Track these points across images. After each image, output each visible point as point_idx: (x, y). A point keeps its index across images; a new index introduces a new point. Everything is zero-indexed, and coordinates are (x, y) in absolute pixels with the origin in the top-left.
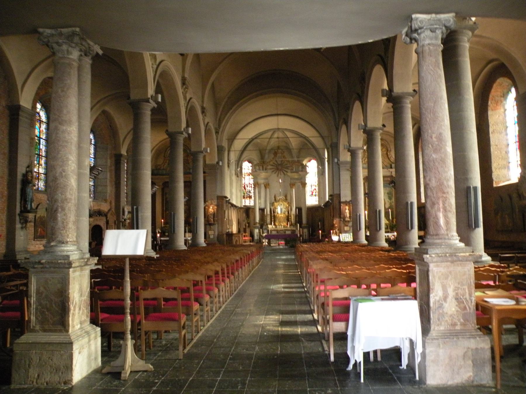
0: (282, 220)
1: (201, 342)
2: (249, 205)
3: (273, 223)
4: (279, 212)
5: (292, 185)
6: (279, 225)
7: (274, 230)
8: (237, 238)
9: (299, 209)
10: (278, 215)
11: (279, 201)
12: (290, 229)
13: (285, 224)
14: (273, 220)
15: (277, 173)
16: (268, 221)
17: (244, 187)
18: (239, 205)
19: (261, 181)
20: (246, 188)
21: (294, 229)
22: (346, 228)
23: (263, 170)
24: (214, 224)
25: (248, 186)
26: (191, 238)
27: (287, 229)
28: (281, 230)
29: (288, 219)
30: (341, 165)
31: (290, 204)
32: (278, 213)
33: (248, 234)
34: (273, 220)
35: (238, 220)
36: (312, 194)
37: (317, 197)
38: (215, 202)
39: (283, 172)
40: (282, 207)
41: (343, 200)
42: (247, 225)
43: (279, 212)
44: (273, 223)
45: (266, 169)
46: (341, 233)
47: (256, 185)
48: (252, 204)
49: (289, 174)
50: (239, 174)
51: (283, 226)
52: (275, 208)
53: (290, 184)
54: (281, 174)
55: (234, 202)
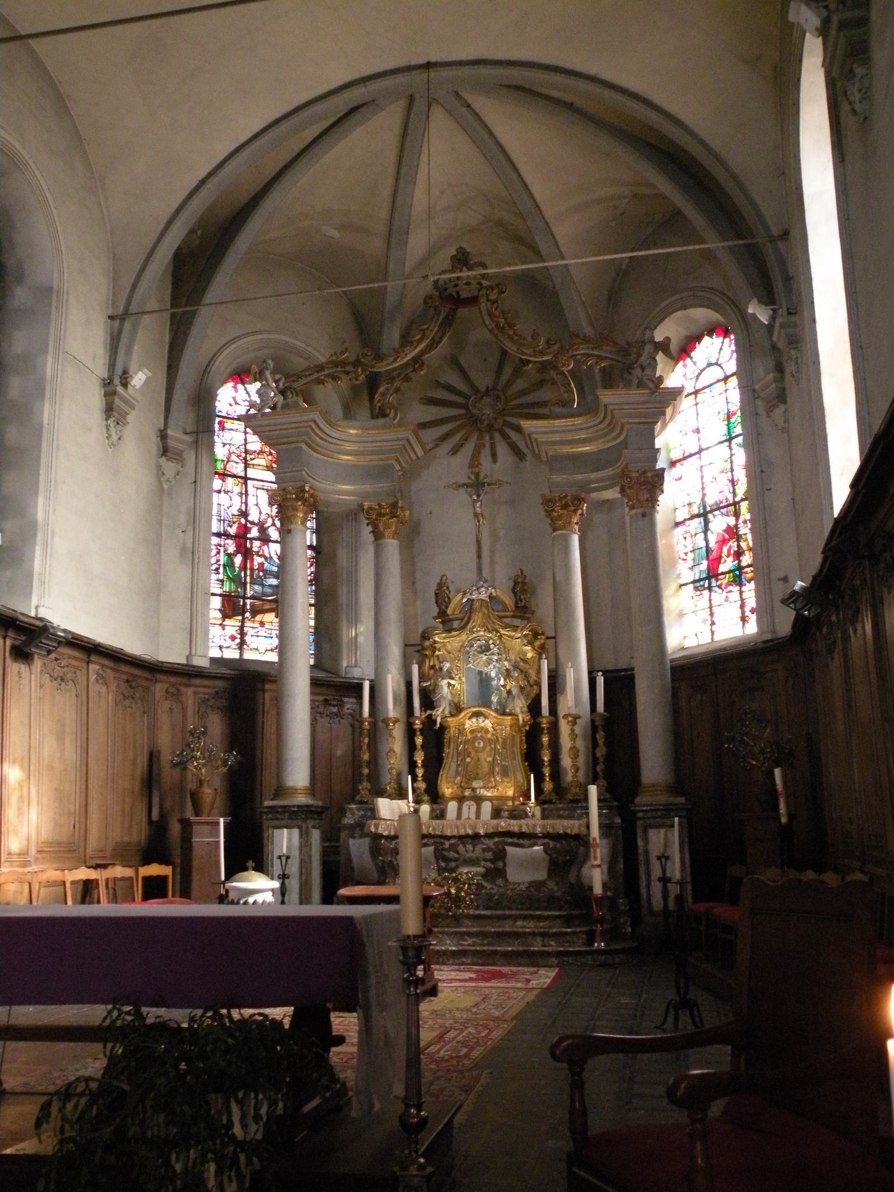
0: (486, 758)
6: (461, 800)
11: (464, 624)
15: (468, 449)
17: (241, 537)
26: (432, 833)
35: (153, 757)
36: (713, 573)
39: (505, 437)
51: (487, 807)
53: (548, 503)
54: (494, 456)
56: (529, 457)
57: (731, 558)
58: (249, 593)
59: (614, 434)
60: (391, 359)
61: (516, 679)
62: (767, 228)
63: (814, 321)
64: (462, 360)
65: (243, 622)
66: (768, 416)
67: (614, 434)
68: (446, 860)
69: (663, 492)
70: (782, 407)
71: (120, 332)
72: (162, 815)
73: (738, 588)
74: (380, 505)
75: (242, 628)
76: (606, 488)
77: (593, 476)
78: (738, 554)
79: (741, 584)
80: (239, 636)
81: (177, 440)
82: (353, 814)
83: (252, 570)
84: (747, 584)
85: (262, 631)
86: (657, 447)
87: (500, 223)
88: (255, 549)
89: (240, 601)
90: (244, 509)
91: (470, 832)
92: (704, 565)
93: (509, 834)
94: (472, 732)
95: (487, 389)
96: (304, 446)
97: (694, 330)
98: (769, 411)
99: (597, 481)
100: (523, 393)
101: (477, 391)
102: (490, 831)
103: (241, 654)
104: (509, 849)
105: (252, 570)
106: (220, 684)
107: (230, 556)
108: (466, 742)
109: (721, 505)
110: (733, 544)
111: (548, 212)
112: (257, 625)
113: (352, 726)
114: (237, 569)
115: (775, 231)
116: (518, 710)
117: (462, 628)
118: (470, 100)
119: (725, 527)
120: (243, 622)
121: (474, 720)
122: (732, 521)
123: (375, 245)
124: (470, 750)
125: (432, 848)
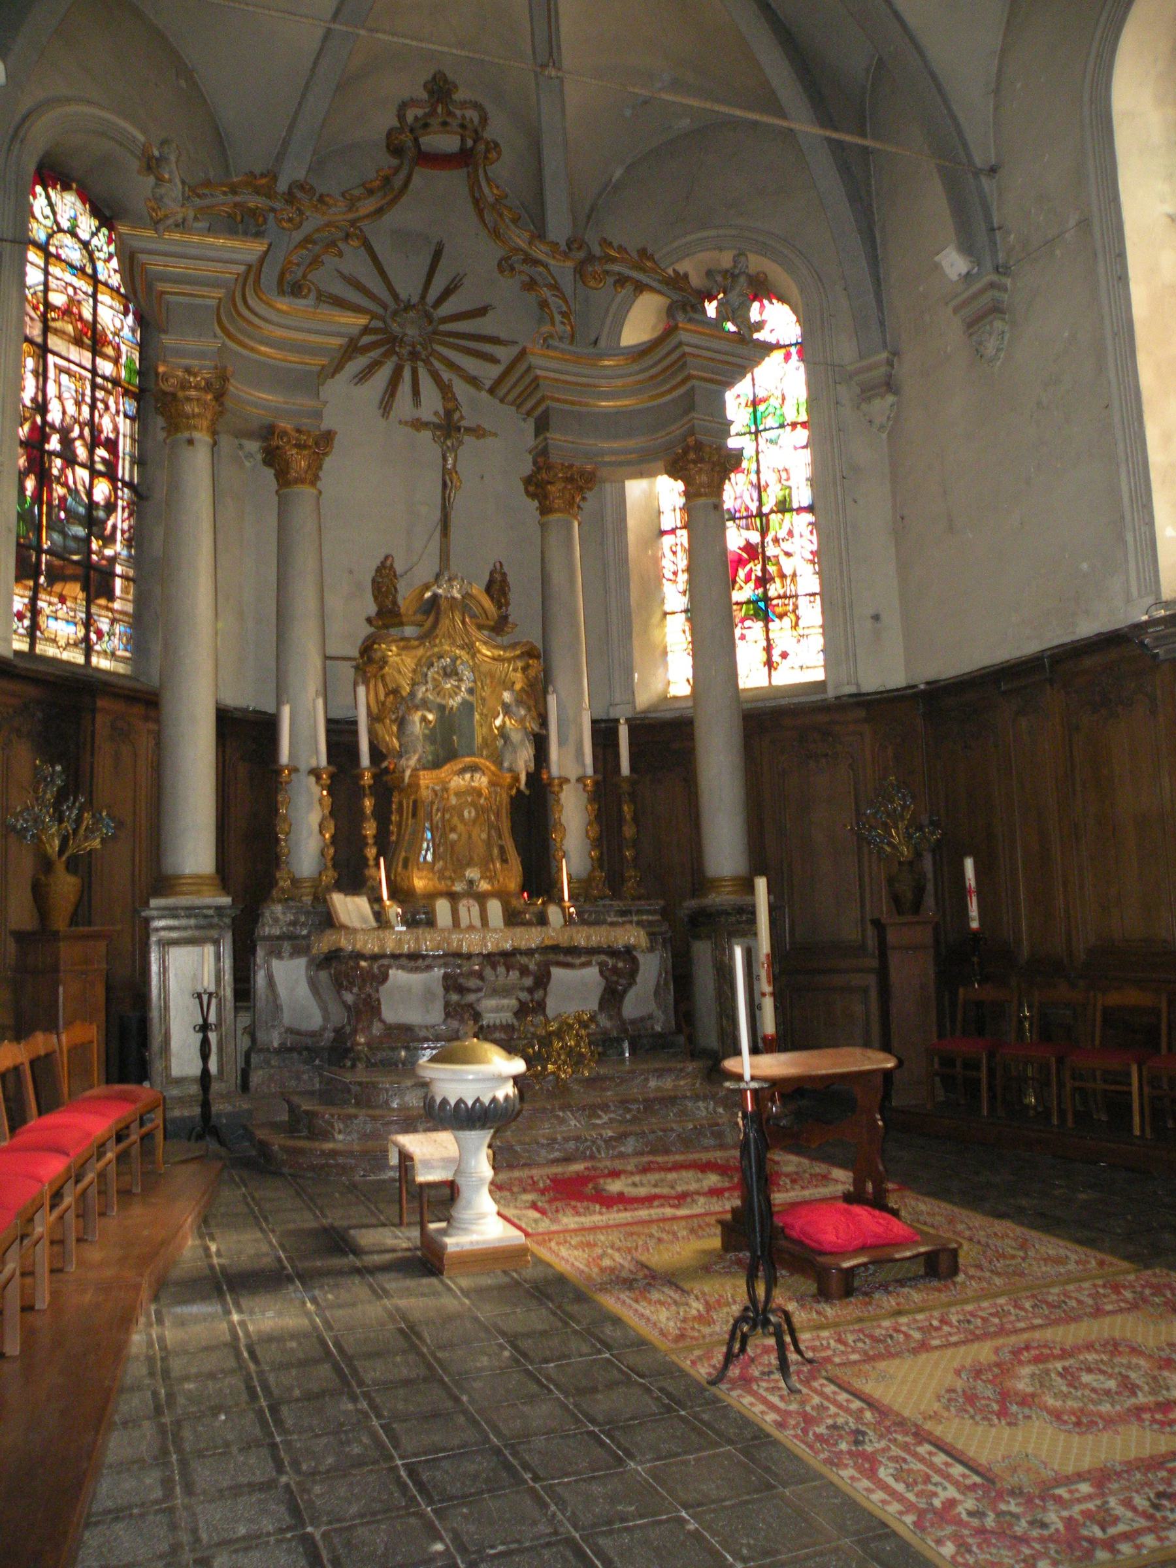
6: (453, 897)
15: (383, 375)
54: (416, 392)
57: (752, 584)
69: (807, 479)
73: (761, 624)
75: (34, 600)
79: (767, 620)
80: (29, 615)
83: (50, 505)
84: (777, 620)
85: (63, 611)
88: (55, 472)
89: (31, 556)
90: (40, 399)
94: (458, 794)
99: (613, 452)
103: (32, 645)
105: (50, 505)
109: (737, 515)
112: (55, 600)
114: (29, 499)
119: (742, 544)
122: (754, 537)
124: (455, 820)
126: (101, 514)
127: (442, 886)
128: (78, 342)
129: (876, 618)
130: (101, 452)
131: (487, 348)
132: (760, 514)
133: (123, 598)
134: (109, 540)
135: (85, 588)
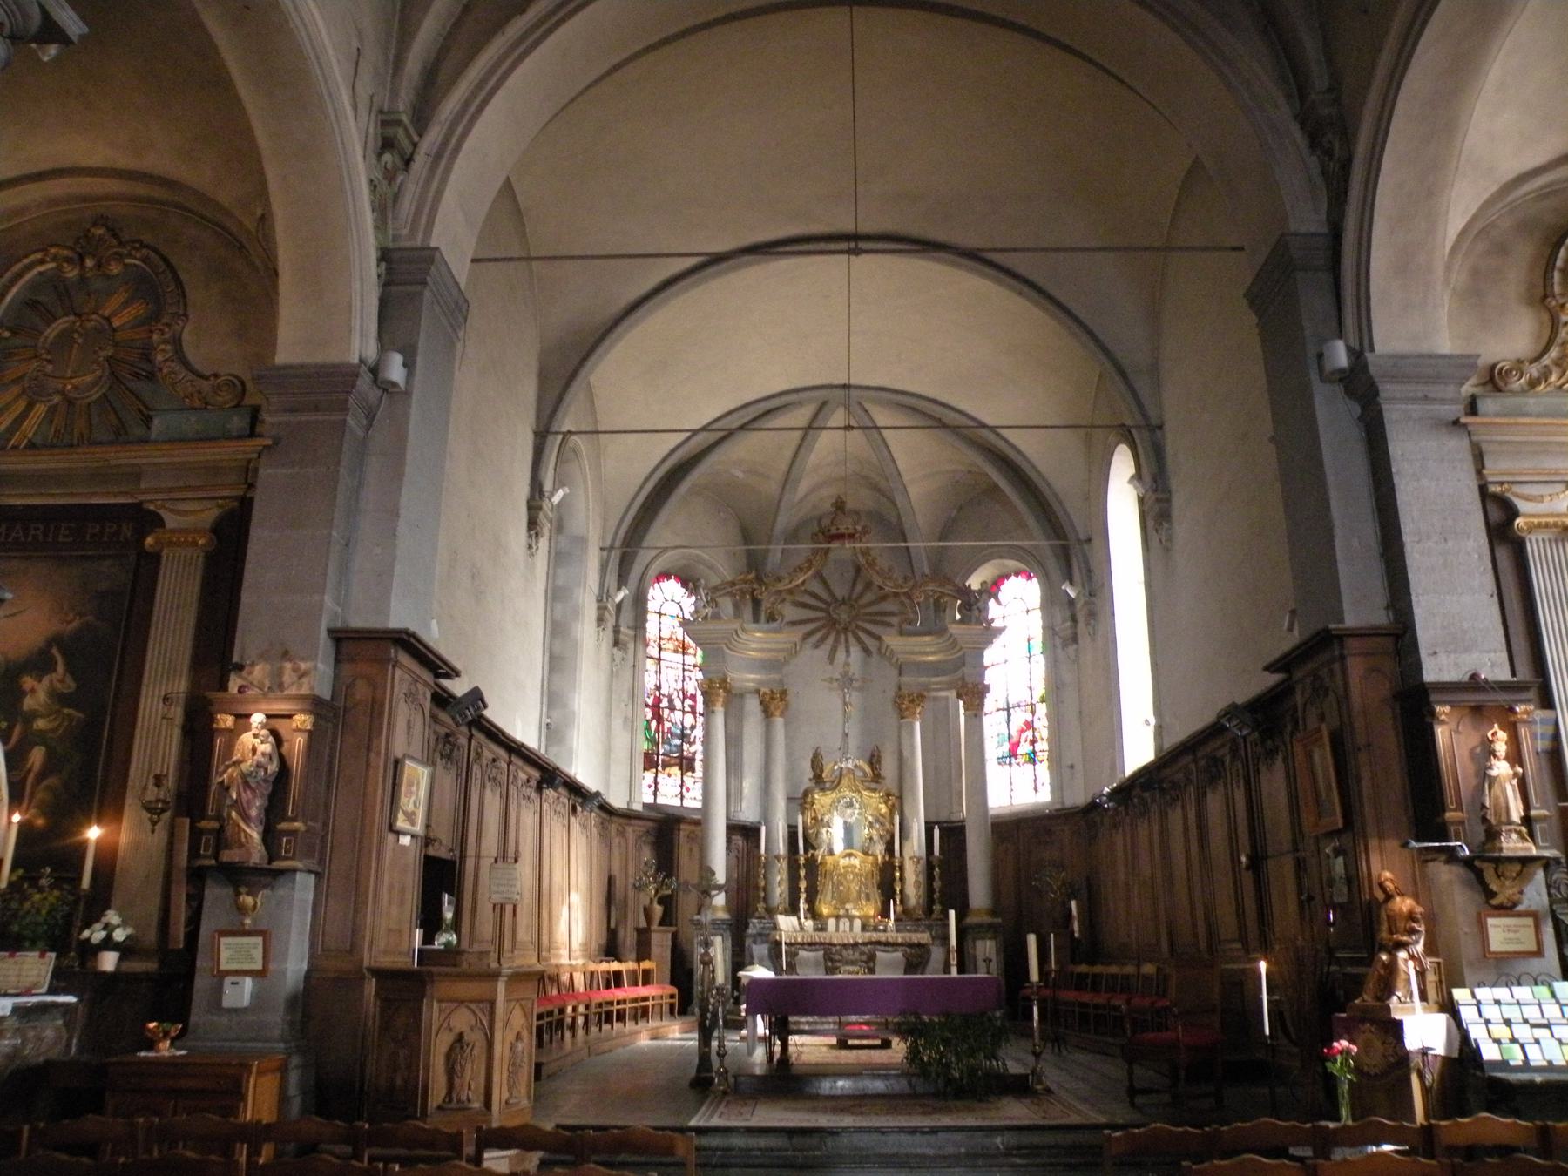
1: (1048, 539)
2: (676, 802)
3: (803, 906)
4: (839, 847)
5: (906, 703)
6: (838, 917)
7: (811, 945)
8: (462, 1020)
9: (951, 835)
10: (829, 859)
11: (836, 785)
12: (900, 938)
13: (871, 910)
14: (803, 885)
16: (779, 891)
17: (656, 708)
18: (617, 801)
19: (746, 679)
20: (666, 713)
21: (923, 937)
22: (1502, 933)
23: (756, 619)
24: (270, 875)
25: (678, 704)
27: (882, 937)
28: (845, 946)
29: (886, 881)
30: (1387, 390)
31: (898, 801)
32: (831, 853)
33: (657, 963)
34: (803, 885)
35: (611, 881)
36: (1013, 753)
37: (1043, 771)
38: (319, 675)
40: (853, 815)
41: (1435, 669)
42: (658, 910)
43: (839, 847)
44: (803, 906)
45: (771, 618)
46: (1452, 977)
47: (716, 689)
48: (693, 800)
49: (893, 641)
50: (390, 204)
51: (857, 923)
52: (819, 822)
54: (848, 651)
55: (584, 771)
56: (875, 655)
58: (661, 751)
59: (956, 650)
60: (787, 581)
61: (877, 830)
62: (1077, 534)
63: (1113, 614)
64: (825, 573)
65: (656, 774)
66: (1063, 649)
67: (956, 650)
68: (832, 960)
70: (1075, 646)
71: (608, 561)
72: (616, 926)
74: (772, 692)
76: (947, 689)
77: (933, 680)
78: (1033, 742)
81: (626, 635)
82: (755, 927)
86: (1250, 872)
87: (866, 478)
88: (665, 716)
91: (851, 941)
92: (1006, 747)
93: (879, 943)
95: (844, 599)
96: (724, 646)
97: (1005, 571)
98: (1064, 646)
99: (937, 683)
100: (872, 603)
101: (836, 600)
102: (866, 940)
104: (878, 953)
106: (650, 824)
107: (649, 722)
108: (840, 875)
110: (1029, 734)
111: (906, 478)
113: (737, 857)
115: (1082, 537)
116: (878, 852)
117: (833, 789)
118: (867, 408)
120: (656, 774)
121: (847, 859)
123: (772, 487)
124: (843, 880)
125: (822, 953)
126: (688, 732)
127: (835, 912)
128: (676, 651)
129: (1072, 767)
130: (688, 702)
131: (887, 619)
132: (1032, 705)
133: (699, 772)
134: (691, 744)
135: (681, 769)
